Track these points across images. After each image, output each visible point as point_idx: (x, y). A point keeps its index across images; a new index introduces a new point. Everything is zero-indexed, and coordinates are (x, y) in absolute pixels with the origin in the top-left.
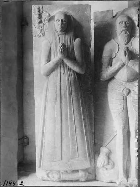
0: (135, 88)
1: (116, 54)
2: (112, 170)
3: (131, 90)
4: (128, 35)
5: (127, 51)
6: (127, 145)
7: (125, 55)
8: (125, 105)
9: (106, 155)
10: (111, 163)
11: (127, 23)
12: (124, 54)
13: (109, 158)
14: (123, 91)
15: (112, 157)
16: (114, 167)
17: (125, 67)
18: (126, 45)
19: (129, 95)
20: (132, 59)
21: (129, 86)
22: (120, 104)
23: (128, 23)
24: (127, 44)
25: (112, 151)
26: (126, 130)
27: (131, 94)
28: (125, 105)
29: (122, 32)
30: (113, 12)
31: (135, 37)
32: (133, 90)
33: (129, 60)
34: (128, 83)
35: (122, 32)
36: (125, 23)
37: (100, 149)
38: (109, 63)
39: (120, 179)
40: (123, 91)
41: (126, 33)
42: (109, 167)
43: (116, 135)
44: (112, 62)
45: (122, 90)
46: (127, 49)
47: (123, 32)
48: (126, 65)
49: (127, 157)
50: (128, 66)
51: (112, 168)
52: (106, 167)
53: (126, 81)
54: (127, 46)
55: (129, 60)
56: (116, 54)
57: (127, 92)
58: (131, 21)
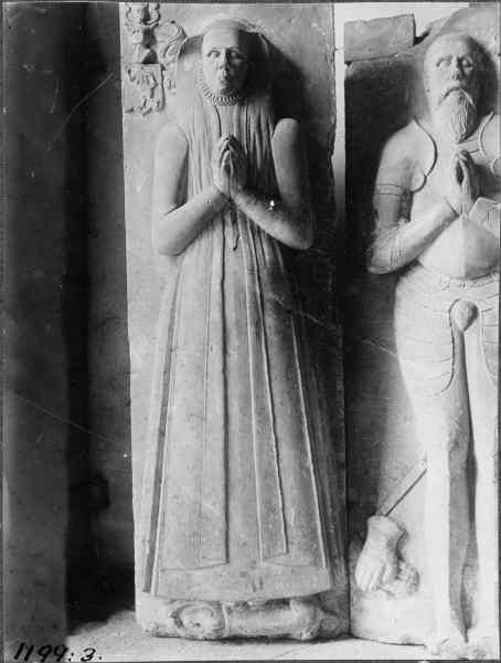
1: (426, 177)
2: (412, 600)
3: (480, 310)
6: (463, 501)
7: (460, 179)
9: (389, 544)
10: (406, 573)
11: (464, 63)
14: (450, 311)
15: (409, 550)
16: (416, 590)
17: (458, 223)
23: (471, 62)
25: (409, 530)
26: (464, 452)
29: (447, 95)
34: (469, 283)
36: (460, 61)
39: (442, 636)
40: (450, 311)
41: (462, 98)
42: (400, 587)
43: (424, 473)
44: (410, 202)
45: (447, 308)
46: (465, 159)
47: (454, 97)
48: (461, 217)
49: (463, 553)
50: (469, 220)
51: (410, 593)
52: (387, 587)
55: (474, 197)
56: (426, 177)
57: (467, 316)
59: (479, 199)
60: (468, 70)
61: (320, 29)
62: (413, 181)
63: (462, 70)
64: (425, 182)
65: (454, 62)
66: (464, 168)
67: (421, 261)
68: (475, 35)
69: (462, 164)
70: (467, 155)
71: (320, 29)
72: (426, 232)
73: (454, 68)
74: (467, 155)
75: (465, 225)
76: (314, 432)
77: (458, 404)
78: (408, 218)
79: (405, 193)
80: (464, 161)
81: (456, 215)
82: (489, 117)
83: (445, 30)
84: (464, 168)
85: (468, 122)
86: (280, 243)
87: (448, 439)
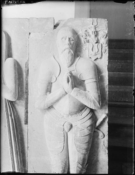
0: (78, 122)
1: (56, 78)
3: (73, 126)
4: (72, 54)
5: (71, 77)
7: (68, 82)
8: (65, 143)
11: (71, 39)
12: (66, 81)
13: (86, 97)
14: (63, 126)
17: (67, 96)
18: (70, 68)
19: (71, 131)
20: (75, 86)
21: (72, 120)
22: (59, 142)
23: (73, 39)
24: (71, 65)
27: (73, 130)
28: (65, 143)
29: (65, 50)
30: (54, 20)
31: (80, 57)
32: (75, 125)
33: (73, 88)
34: (70, 116)
35: (65, 50)
36: (69, 39)
37: (104, 18)
38: (48, 89)
40: (63, 126)
41: (70, 52)
44: (51, 87)
45: (63, 125)
46: (70, 75)
47: (67, 51)
48: (68, 94)
50: (71, 95)
53: (68, 113)
54: (71, 69)
55: (73, 88)
56: (56, 78)
57: (69, 128)
58: (77, 36)
59: (74, 88)
60: (72, 42)
61: (25, 29)
62: (52, 79)
63: (70, 42)
64: (56, 80)
65: (67, 39)
66: (70, 78)
67: (54, 106)
68: (75, 28)
69: (69, 77)
70: (71, 73)
71: (25, 29)
72: (56, 99)
73: (67, 41)
74: (71, 73)
75: (69, 97)
76: (17, 132)
77: (65, 157)
78: (50, 92)
79: (49, 83)
80: (70, 76)
81: (66, 93)
82: (79, 58)
83: (65, 25)
84: (70, 78)
85: (72, 60)
86: (10, 101)
87: (61, 169)
